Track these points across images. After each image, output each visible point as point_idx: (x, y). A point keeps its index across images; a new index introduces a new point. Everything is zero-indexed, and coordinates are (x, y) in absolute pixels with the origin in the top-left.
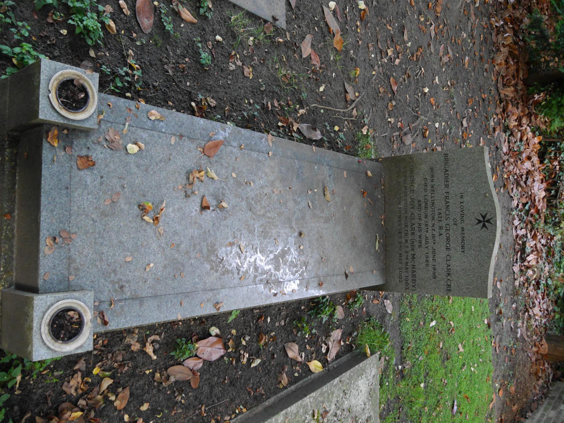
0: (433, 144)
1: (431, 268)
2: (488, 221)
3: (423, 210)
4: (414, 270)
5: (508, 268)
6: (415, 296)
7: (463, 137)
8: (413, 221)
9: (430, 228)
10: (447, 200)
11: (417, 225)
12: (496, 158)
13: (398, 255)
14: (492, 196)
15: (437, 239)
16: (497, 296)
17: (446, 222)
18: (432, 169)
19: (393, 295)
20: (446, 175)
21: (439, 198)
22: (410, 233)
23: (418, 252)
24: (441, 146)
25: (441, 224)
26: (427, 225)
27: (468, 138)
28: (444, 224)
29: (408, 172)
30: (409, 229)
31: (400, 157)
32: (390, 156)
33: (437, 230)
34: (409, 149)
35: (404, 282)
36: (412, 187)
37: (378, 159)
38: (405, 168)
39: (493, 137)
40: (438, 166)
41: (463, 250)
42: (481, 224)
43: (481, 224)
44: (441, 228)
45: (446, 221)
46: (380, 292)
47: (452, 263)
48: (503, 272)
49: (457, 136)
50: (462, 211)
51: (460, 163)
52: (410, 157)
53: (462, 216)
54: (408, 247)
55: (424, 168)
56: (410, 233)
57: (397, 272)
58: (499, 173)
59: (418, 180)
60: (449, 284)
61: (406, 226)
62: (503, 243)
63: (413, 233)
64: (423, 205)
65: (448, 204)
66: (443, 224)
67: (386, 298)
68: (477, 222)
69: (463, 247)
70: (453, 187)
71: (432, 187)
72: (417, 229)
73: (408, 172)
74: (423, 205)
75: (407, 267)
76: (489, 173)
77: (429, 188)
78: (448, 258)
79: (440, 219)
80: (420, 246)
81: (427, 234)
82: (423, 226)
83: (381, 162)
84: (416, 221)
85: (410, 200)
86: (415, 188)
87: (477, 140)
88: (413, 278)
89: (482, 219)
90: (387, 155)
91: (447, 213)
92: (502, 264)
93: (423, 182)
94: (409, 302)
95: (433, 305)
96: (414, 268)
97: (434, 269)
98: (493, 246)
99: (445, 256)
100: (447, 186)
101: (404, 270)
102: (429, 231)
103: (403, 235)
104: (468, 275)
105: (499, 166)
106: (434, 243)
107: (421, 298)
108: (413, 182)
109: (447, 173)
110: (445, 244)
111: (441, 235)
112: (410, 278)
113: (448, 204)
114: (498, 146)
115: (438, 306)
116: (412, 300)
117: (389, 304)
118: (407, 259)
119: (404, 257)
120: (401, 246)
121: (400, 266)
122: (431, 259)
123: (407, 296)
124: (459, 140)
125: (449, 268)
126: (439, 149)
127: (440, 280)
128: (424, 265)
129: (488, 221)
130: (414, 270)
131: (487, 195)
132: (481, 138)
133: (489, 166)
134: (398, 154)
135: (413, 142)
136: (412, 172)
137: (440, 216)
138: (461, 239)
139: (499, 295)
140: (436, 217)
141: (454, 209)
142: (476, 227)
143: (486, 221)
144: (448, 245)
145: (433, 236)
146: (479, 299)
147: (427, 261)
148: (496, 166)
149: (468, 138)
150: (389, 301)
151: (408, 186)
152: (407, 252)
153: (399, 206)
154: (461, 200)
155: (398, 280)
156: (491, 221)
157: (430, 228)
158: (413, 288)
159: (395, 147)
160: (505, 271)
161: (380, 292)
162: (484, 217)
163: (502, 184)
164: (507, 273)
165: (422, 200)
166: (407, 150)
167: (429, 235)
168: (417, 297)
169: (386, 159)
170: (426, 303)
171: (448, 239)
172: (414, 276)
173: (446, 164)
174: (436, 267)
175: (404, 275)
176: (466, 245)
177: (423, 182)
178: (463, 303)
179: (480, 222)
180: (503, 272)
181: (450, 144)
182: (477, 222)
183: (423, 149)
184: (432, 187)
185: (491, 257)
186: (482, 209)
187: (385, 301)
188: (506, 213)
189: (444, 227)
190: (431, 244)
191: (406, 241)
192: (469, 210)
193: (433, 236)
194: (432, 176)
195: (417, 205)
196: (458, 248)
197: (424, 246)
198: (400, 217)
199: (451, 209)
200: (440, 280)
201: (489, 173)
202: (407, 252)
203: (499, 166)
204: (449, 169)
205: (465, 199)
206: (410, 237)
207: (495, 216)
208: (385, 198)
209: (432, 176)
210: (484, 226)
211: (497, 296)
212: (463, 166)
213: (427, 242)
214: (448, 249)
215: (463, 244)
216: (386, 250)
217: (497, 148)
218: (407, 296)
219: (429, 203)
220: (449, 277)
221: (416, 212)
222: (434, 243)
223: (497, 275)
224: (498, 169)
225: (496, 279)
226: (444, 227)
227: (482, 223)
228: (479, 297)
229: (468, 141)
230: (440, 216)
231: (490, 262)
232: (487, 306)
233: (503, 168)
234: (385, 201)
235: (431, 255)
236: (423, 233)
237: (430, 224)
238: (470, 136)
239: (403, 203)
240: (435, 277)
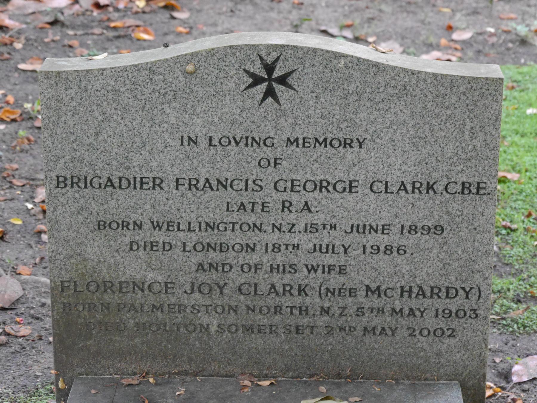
0: (28, 210)
1: (409, 241)
2: (270, 68)
3: (231, 257)
4: (415, 290)
5: (412, 8)
6: (498, 283)
7: (14, 120)
8: (264, 287)
9: (287, 238)
10: (201, 185)
11: (276, 278)
12: (84, 26)
13: (369, 339)
14: (194, 55)
15: (319, 219)
16: (494, 39)
17: (269, 189)
18: (101, 226)
19: (495, 352)
20: (124, 183)
21: (194, 207)
22: (298, 300)
23: (358, 278)
24: (34, 188)
25: (274, 205)
26: (276, 248)
27: (18, 104)
28: (276, 196)
29: (107, 297)
30: (286, 301)
31: (55, 322)
32: (51, 348)
33: (292, 217)
34: (36, 286)
35: (455, 323)
36: (156, 288)
37: (59, 390)
38: (92, 307)
39: (20, 32)
40: (95, 207)
41: (355, 144)
42: (278, 88)
43: (278, 88)
44: (286, 206)
45: (266, 191)
46: (488, 393)
47: (394, 178)
48: (423, 22)
49: (7, 138)
50: (237, 143)
51: (88, 141)
52: (59, 289)
53: (251, 141)
54: (345, 308)
55: (96, 248)
56: (298, 300)
57: (422, 342)
58: (130, 21)
59: (134, 267)
60: (459, 188)
61: (278, 310)
62: (337, 20)
63: (302, 290)
64: (214, 256)
65: (214, 183)
66: (274, 199)
67: (506, 376)
68: (270, 100)
69: (346, 144)
70: (161, 166)
71: (157, 226)
72: (287, 278)
73: (107, 297)
74: (214, 256)
75: (406, 311)
76: (128, 58)
77: (160, 237)
78: (380, 187)
79: (258, 208)
80: (342, 271)
81: (305, 247)
82: (280, 259)
83: (69, 384)
84: (263, 279)
85: (197, 295)
86: (160, 278)
87: (26, 81)
88: (443, 294)
89: (264, 86)
90: (48, 358)
91: (242, 185)
92: (400, 22)
93: (141, 253)
94: (519, 301)
95: (527, 230)
96: (410, 291)
97: (413, 229)
98: (345, 56)
99: (373, 196)
100: (157, 184)
101: (416, 322)
102: (296, 241)
103: (305, 321)
104: (431, 130)
105: (109, 20)
106: (333, 227)
107: (503, 266)
108: (139, 286)
109: (116, 181)
110: (337, 195)
111: (307, 207)
112: (441, 304)
113: (214, 183)
114: (49, 19)
115: (529, 215)
116: (511, 294)
117: (526, 366)
118: (381, 311)
119: (376, 321)
120: (341, 329)
121: (402, 333)
122: (383, 240)
123: (497, 309)
124: (21, 133)
125: (409, 188)
126: (41, 194)
127: (448, 213)
128: (400, 260)
129: (270, 68)
130: (415, 290)
131: (190, 68)
132: (22, 66)
133: (101, 60)
134: (48, 323)
135: (16, 273)
136: (106, 286)
137: (249, 207)
138: (320, 149)
139: (491, 35)
140: (252, 219)
141: (232, 164)
142: (285, 103)
143: (270, 76)
144: (339, 187)
145: (311, 228)
146: (505, 93)
147: (388, 250)
148: (108, 28)
149: (18, 104)
150: (516, 368)
151: (152, 299)
152: (360, 312)
153: (213, 329)
154: (203, 143)
155: (447, 341)
156: (269, 60)
157: (287, 238)
158: (473, 298)
159: (24, 331)
160: (421, 16)
161: (488, 393)
162: (257, 80)
163: (166, 14)
164: (428, 9)
165: (199, 257)
166: (40, 294)
167: (307, 242)
168: (501, 276)
169: (60, 364)
170: (517, 251)
171: (321, 186)
172: (435, 292)
173: (88, 183)
174: (407, 225)
175: (430, 322)
176: (341, 136)
177: (141, 253)
178: (517, 138)
179: (270, 93)
180: (423, 22)
181: (31, 161)
182: (270, 100)
183: (40, 242)
184: (157, 226)
185: (376, 65)
186: (231, 85)
187: (515, 379)
188: (250, 7)
189: (285, 196)
190: (338, 238)
191: (325, 311)
192: (233, 122)
193: (311, 228)
194: (125, 225)
195: (214, 275)
196: (349, 157)
197: (342, 260)
198: (249, 329)
199: (229, 176)
200: (448, 213)
201: (128, 58)
202: (360, 312)
203: (109, 20)
204: (105, 174)
205: (198, 128)
206: (313, 300)
207: (255, 47)
208: (186, 373)
209: (125, 225)
210: (283, 80)
211: (494, 39)
212: (97, 134)
213: (331, 249)
214: (351, 188)
215: (336, 143)
216: (353, 377)
217: (54, 23)
218: (497, 309)
219: (208, 237)
220: (440, 187)
221: (236, 278)
222: (333, 227)
223: (432, 40)
224: (118, 24)
225: (443, 41)
226: (285, 196)
227: (275, 85)
228: (501, 94)
229: (28, 106)
230: (249, 207)
231: (394, 68)
232: (525, 69)
233: (117, 10)
234: (195, 374)
235: (371, 239)
236: (302, 258)
237: (274, 237)
238: (11, 99)
239: (205, 319)
240: (440, 229)
